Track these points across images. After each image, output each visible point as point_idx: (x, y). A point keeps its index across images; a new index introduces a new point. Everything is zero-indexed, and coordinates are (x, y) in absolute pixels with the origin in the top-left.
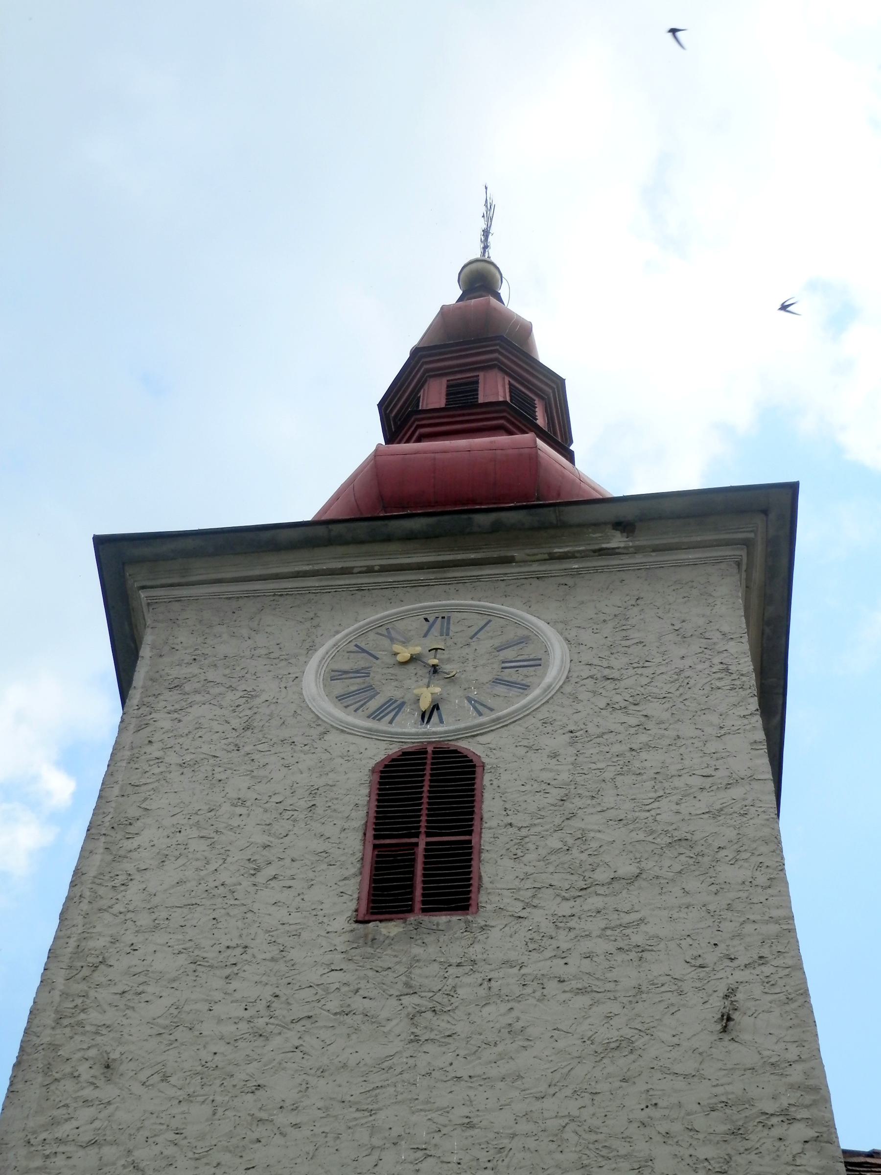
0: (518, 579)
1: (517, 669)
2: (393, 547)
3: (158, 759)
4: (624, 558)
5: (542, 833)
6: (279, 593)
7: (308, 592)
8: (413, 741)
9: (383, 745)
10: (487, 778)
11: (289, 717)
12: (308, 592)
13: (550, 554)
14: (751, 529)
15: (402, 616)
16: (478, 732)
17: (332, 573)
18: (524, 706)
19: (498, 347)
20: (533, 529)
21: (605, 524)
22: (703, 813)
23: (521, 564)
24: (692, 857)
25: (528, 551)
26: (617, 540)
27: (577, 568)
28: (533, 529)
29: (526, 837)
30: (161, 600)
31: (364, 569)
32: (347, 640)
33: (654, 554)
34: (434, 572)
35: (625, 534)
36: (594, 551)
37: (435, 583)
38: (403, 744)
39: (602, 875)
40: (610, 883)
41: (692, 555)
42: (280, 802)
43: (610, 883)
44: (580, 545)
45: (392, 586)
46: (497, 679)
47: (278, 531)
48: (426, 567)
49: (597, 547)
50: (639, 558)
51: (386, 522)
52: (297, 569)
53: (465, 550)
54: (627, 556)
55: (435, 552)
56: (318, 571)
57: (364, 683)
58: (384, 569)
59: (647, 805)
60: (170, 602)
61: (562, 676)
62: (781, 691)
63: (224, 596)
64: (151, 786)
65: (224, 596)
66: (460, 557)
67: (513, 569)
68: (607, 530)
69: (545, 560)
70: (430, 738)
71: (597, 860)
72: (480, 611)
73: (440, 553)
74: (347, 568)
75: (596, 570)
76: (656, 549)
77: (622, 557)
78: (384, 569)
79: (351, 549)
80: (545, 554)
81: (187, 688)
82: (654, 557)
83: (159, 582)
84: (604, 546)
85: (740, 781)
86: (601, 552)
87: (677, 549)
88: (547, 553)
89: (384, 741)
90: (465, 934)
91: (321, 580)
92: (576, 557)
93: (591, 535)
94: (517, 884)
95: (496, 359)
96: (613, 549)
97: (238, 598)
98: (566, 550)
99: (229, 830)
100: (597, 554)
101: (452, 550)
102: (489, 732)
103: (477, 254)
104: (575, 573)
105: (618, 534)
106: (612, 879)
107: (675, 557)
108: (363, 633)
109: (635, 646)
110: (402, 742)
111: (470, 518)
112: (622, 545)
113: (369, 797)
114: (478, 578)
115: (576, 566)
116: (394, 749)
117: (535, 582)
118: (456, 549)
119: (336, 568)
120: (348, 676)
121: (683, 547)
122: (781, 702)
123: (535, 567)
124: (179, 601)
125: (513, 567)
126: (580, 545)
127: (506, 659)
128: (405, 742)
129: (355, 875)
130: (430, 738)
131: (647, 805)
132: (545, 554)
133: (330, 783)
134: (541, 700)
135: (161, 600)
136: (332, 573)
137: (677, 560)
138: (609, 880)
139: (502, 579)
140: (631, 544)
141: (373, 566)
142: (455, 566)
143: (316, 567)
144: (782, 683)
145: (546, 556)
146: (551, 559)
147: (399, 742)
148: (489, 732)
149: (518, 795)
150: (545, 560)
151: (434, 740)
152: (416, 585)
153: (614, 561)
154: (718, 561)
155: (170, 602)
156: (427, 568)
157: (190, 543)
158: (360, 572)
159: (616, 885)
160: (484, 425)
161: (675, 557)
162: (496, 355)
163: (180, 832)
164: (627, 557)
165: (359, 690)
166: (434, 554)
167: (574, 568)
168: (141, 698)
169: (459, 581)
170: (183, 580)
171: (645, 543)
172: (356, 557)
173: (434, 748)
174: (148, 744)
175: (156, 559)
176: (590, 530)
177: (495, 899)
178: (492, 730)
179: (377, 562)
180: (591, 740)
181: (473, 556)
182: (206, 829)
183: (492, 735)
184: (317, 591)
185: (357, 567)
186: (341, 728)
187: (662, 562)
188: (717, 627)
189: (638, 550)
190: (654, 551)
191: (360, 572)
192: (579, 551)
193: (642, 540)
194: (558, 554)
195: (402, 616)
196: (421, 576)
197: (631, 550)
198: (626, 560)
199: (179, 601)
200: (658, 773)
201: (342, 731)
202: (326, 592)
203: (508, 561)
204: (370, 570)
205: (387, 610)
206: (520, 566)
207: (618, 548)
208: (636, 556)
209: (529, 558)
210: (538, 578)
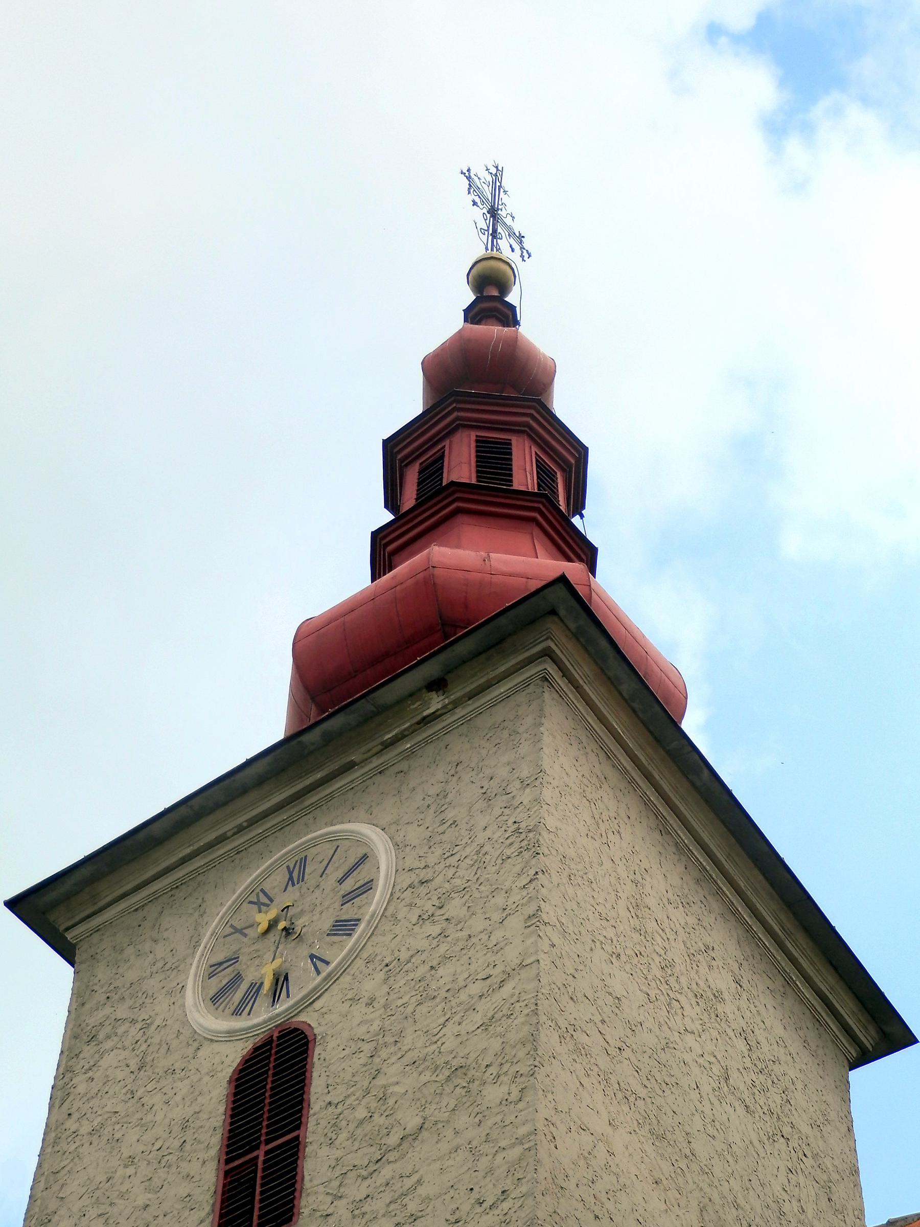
0: (364, 781)
1: (352, 902)
2: (253, 795)
3: (75, 1132)
4: (446, 718)
5: (353, 1103)
6: (175, 886)
7: (197, 874)
8: (263, 1030)
9: (240, 1045)
10: (317, 1050)
11: (174, 1039)
12: (197, 874)
13: (382, 744)
14: (545, 637)
15: (268, 873)
16: (315, 997)
17: (210, 846)
18: (350, 951)
19: (454, 405)
20: (360, 724)
21: (420, 690)
22: (478, 1028)
23: (363, 764)
24: (465, 1087)
25: (364, 749)
26: (436, 702)
27: (410, 747)
28: (360, 724)
29: (340, 1114)
30: (84, 936)
31: (236, 830)
32: (223, 923)
33: (470, 702)
34: (293, 807)
35: (441, 692)
36: (418, 723)
37: (297, 818)
38: (256, 1037)
39: (393, 1139)
40: (400, 1145)
41: (502, 688)
42: (160, 1148)
43: (400, 1145)
44: (403, 724)
45: (263, 837)
46: (337, 921)
47: (148, 828)
48: (285, 804)
49: (419, 718)
50: (460, 712)
51: (232, 778)
52: (181, 855)
53: (311, 772)
54: (448, 715)
55: (286, 786)
56: (198, 849)
57: (233, 971)
58: (253, 822)
59: (436, 1035)
60: (91, 935)
61: (386, 895)
62: (690, 749)
63: (132, 909)
64: (66, 1169)
65: (132, 909)
66: (308, 781)
67: (357, 773)
68: (424, 696)
69: (382, 750)
70: (276, 1022)
71: (391, 1120)
72: (329, 838)
73: (292, 785)
74: (220, 836)
75: (427, 742)
76: (472, 696)
77: (444, 717)
78: (253, 822)
79: (219, 814)
80: (377, 746)
81: (101, 1036)
82: (472, 705)
83: (77, 919)
84: (425, 714)
85: (512, 973)
86: (426, 721)
87: (489, 687)
88: (379, 744)
89: (242, 1039)
90: (691, 995)
91: (205, 857)
92: (407, 736)
93: (412, 707)
94: (329, 1174)
95: (457, 418)
96: (434, 713)
97: (143, 906)
98: (394, 733)
99: (120, 1199)
100: (422, 724)
101: (301, 778)
102: (324, 992)
103: (480, 252)
104: (410, 753)
105: (433, 695)
106: (402, 1138)
107: (488, 698)
108: (236, 909)
109: (449, 829)
110: (255, 1035)
111: (299, 742)
112: (439, 706)
113: (225, 1114)
114: (331, 796)
115: (409, 746)
116: (249, 1045)
117: (379, 778)
118: (304, 774)
119: (211, 840)
120: (222, 967)
121: (494, 683)
122: (697, 757)
123: (376, 762)
124: (98, 930)
125: (356, 771)
126: (404, 722)
127: (346, 891)
128: (257, 1035)
129: (209, 1214)
130: (276, 1022)
131: (436, 1035)
132: (377, 746)
133: (197, 1110)
134: (367, 935)
135: (84, 936)
136: (210, 846)
137: (491, 699)
138: (399, 1141)
139: (351, 787)
140: (447, 701)
141: (241, 825)
142: (309, 792)
143: (196, 846)
144: (685, 742)
145: (380, 747)
146: (386, 747)
147: (253, 1036)
148: (324, 992)
149: (339, 1063)
150: (382, 750)
151: (279, 1022)
152: (281, 827)
153: (438, 726)
154: (526, 684)
155: (91, 935)
156: (287, 805)
157: (84, 872)
158: (235, 834)
159: (405, 1145)
160: (440, 517)
161: (488, 698)
162: (455, 414)
163: (84, 1215)
164: (449, 716)
165: (230, 981)
166: (287, 788)
167: (407, 749)
168: (67, 1062)
169: (317, 806)
170: (96, 908)
171: (459, 694)
172: (224, 821)
173: (280, 1032)
174: (68, 1118)
175: (67, 897)
176: (409, 702)
177: (311, 1199)
178: (326, 990)
179: (242, 819)
180: (402, 969)
181: (319, 776)
182: (104, 1204)
183: (326, 995)
184: (204, 870)
185: (228, 831)
186: (210, 1037)
187: (480, 707)
188: (516, 776)
189: (456, 704)
190: (469, 699)
191: (235, 834)
192: (406, 729)
193: (457, 693)
194: (389, 740)
195: (268, 873)
196: (283, 816)
197: (450, 707)
198: (449, 719)
199: (98, 930)
200: (449, 990)
201: (212, 1040)
202: (212, 867)
203: (350, 767)
204: (240, 829)
205: (251, 875)
206: (362, 767)
207: (438, 710)
208: (457, 710)
209: (366, 756)
210: (380, 773)
